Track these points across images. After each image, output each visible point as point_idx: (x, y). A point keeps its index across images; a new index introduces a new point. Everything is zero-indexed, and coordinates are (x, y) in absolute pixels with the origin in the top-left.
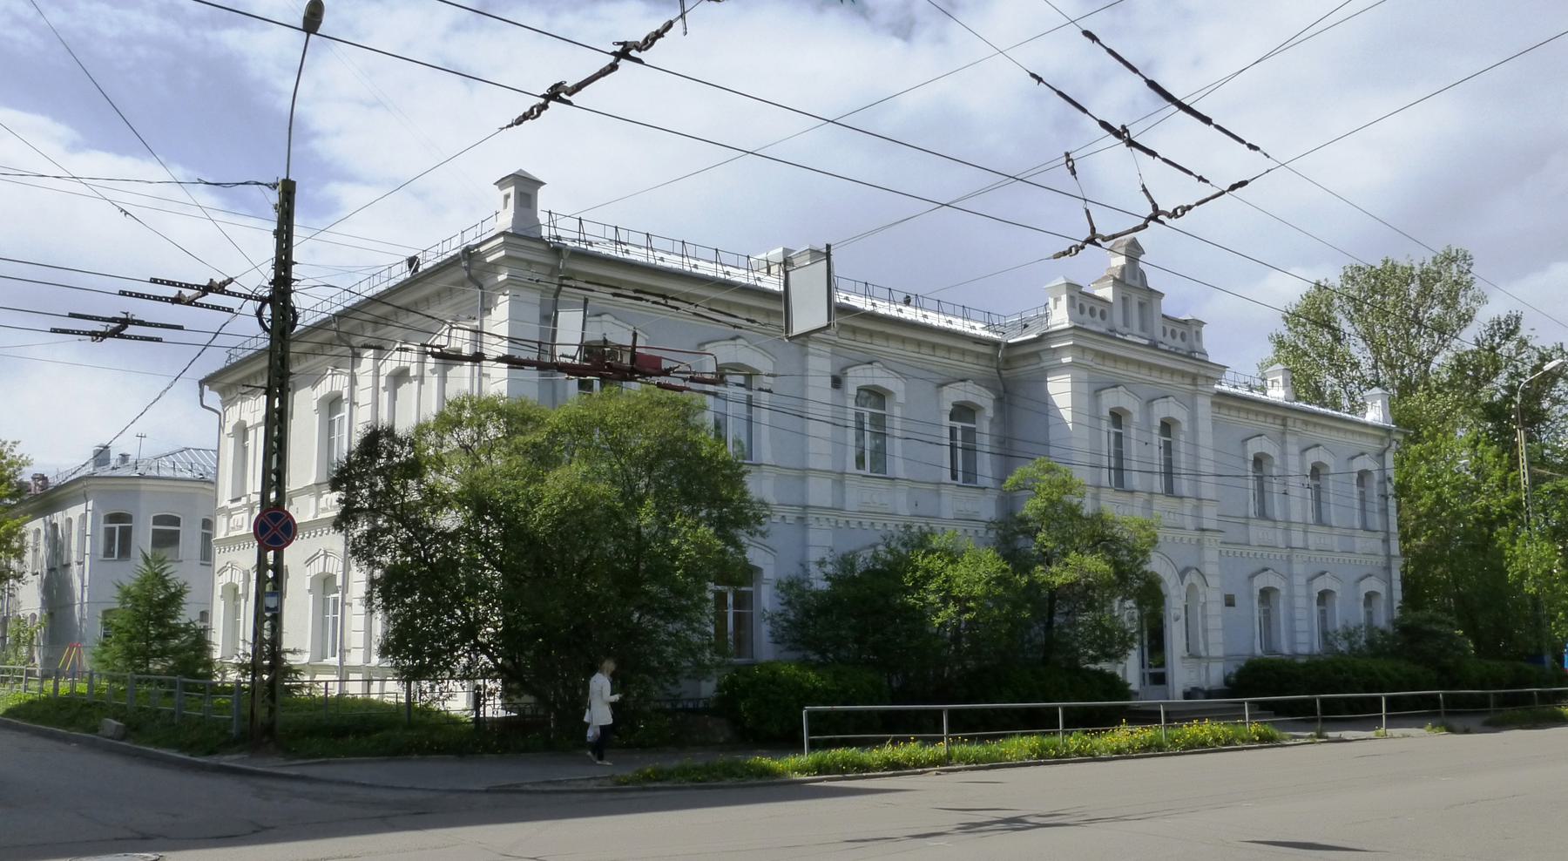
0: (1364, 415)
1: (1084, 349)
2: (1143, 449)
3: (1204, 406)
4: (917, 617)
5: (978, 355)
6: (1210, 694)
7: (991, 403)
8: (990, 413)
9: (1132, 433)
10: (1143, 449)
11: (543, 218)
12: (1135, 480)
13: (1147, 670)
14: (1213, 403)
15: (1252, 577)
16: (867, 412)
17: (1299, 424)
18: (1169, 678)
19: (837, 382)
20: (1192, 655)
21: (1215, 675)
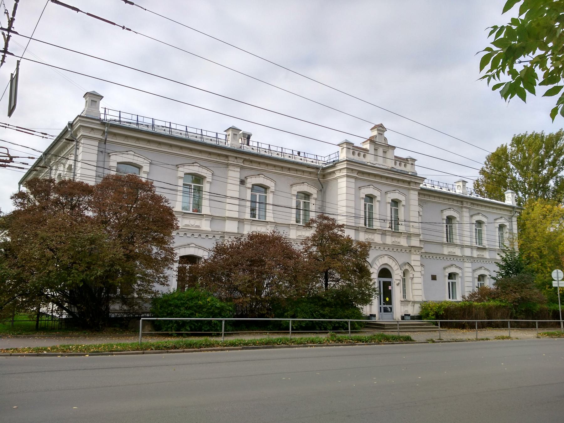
0: (504, 201)
1: (352, 170)
2: (382, 210)
3: (414, 196)
4: (141, 181)
5: (310, 173)
6: (413, 318)
7: (316, 192)
8: (315, 196)
9: (376, 206)
10: (382, 210)
11: (102, 111)
12: (377, 225)
13: (383, 306)
14: (419, 194)
15: (445, 268)
16: (302, 201)
17: (469, 204)
18: (394, 310)
19: (242, 182)
20: (405, 302)
21: (415, 310)
